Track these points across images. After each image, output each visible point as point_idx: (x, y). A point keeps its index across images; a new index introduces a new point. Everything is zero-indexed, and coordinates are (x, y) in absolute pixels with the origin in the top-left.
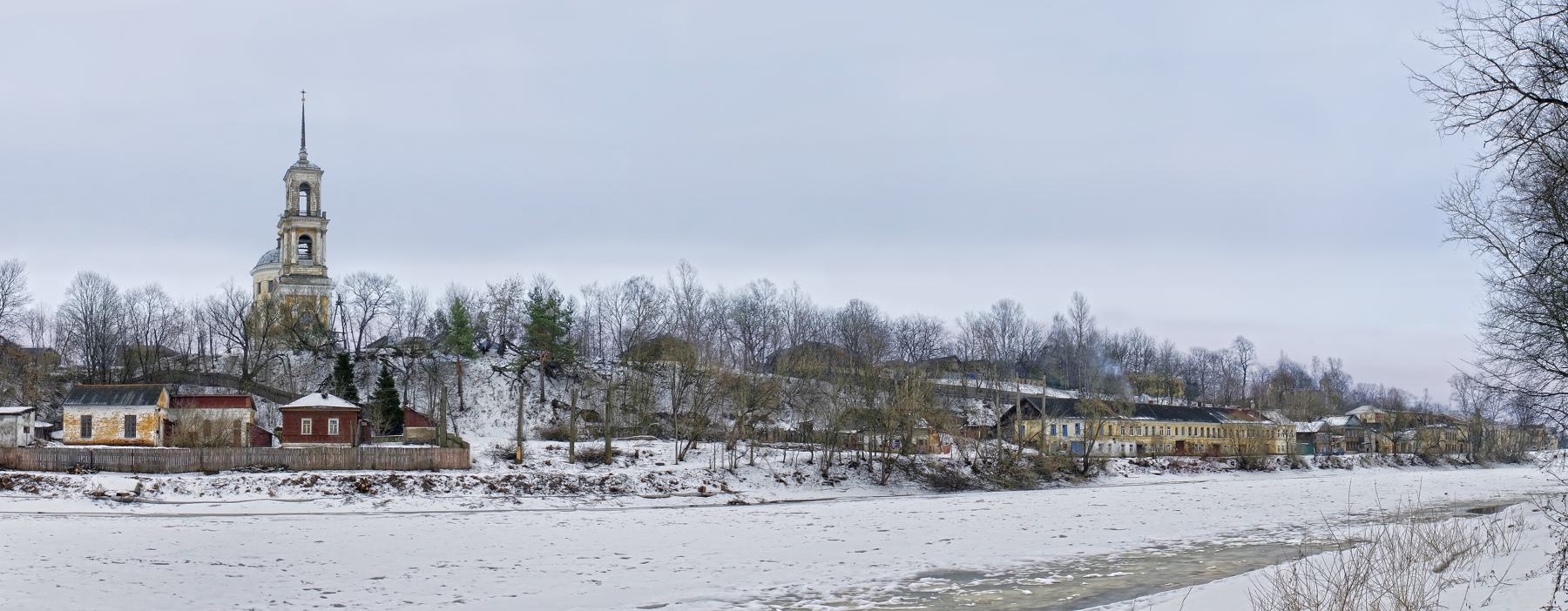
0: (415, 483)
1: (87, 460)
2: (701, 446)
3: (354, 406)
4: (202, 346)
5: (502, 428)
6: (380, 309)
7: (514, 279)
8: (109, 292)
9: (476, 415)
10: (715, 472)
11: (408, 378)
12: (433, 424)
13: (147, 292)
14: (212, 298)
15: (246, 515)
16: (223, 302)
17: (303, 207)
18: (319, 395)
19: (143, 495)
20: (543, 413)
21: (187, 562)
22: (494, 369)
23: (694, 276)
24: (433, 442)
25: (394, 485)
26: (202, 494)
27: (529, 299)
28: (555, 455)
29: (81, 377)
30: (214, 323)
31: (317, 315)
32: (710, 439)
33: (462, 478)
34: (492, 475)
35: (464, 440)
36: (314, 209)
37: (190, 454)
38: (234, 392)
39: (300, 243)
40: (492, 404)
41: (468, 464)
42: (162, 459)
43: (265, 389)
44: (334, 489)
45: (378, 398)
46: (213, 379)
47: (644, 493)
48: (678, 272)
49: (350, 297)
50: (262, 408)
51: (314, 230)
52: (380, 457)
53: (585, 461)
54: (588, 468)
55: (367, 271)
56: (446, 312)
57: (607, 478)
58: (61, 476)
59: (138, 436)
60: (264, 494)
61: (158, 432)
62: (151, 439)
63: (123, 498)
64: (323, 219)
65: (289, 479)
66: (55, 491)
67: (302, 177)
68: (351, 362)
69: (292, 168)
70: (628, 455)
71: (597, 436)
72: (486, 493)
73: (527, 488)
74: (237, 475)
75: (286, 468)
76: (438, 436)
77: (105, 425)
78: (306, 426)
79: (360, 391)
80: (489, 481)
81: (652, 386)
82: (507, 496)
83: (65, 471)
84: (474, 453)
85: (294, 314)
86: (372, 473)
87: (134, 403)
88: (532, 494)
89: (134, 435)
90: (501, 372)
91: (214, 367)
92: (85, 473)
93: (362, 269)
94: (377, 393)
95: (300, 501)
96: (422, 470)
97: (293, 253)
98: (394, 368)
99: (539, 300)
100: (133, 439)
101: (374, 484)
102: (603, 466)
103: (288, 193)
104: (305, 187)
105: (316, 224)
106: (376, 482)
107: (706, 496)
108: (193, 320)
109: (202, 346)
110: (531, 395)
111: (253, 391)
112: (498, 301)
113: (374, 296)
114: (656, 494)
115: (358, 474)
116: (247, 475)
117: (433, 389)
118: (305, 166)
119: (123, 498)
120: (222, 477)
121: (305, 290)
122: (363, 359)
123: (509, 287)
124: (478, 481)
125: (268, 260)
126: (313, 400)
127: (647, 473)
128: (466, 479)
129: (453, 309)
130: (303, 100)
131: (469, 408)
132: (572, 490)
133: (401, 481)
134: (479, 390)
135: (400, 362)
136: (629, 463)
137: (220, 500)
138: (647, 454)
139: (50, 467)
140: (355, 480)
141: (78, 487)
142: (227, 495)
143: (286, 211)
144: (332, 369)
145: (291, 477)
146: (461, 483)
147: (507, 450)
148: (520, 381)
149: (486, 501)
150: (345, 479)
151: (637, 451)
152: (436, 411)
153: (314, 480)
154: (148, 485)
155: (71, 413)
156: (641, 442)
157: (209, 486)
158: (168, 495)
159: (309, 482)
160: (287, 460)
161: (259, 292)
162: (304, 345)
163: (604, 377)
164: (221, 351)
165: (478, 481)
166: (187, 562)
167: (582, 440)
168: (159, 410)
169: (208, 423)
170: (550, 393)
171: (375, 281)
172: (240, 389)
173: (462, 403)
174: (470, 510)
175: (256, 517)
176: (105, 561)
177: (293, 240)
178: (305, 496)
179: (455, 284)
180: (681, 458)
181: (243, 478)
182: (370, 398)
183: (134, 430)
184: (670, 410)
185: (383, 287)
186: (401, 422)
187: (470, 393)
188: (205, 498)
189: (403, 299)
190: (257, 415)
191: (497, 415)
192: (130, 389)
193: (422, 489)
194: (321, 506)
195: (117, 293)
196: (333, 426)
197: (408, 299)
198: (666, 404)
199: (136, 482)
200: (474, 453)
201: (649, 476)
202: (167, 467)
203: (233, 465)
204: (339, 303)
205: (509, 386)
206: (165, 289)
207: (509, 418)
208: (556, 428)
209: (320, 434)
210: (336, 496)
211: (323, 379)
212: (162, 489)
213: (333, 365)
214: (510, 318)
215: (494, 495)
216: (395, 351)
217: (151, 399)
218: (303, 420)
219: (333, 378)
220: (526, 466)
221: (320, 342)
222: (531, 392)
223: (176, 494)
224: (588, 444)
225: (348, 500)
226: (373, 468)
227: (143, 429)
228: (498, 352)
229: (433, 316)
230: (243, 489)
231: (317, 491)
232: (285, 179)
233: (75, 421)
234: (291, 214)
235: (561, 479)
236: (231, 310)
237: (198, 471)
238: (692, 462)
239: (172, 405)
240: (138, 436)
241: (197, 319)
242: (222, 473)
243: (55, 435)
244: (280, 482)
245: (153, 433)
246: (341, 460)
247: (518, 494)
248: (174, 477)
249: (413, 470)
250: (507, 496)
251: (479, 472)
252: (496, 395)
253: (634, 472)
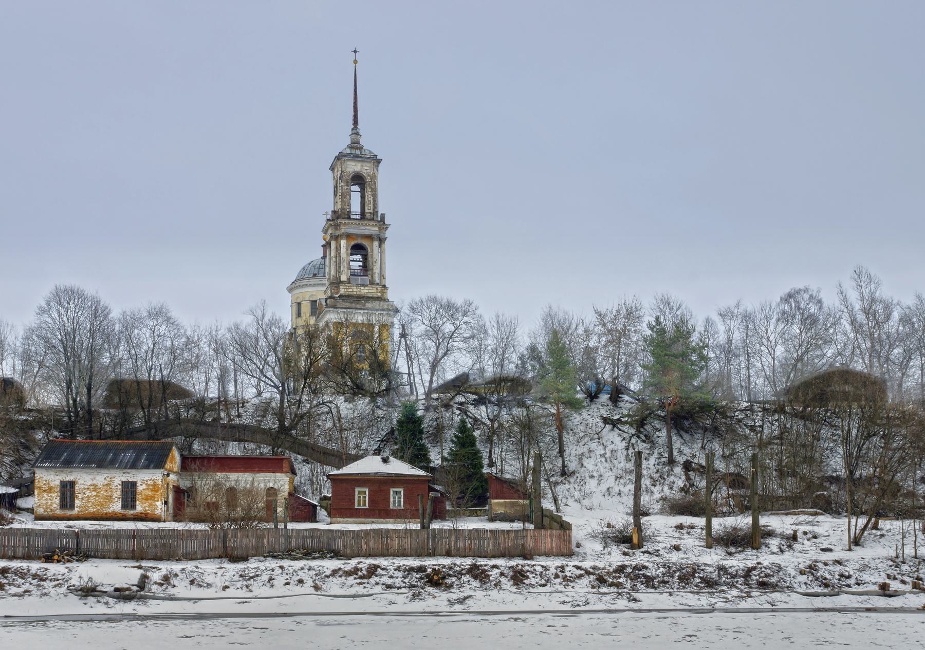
0: (502, 574)
1: (72, 544)
2: (885, 524)
3: (422, 473)
4: (223, 388)
5: (616, 499)
6: (456, 344)
7: (629, 302)
8: (98, 312)
9: (582, 482)
10: (904, 562)
11: (494, 433)
12: (525, 496)
13: (150, 315)
15: (285, 615)
16: (252, 331)
17: (356, 208)
18: (378, 458)
19: (150, 590)
20: (672, 478)
22: (606, 421)
23: (876, 288)
24: (525, 519)
25: (475, 577)
26: (225, 588)
27: (649, 332)
28: (686, 536)
29: (58, 424)
30: (239, 358)
31: (375, 351)
32: (902, 514)
33: (562, 568)
34: (601, 565)
36: (369, 210)
37: (210, 536)
38: (266, 450)
39: (352, 254)
40: (603, 467)
42: (172, 542)
43: (307, 445)
44: (398, 582)
46: (240, 433)
47: (803, 589)
48: (854, 284)
49: (418, 328)
50: (304, 471)
51: (370, 237)
52: (456, 540)
53: (727, 545)
54: (730, 554)
55: (439, 296)
56: (542, 347)
57: (754, 568)
58: (35, 566)
59: (139, 508)
60: (308, 588)
61: (166, 503)
62: (158, 512)
63: (122, 595)
64: (382, 224)
65: (340, 569)
66: (27, 587)
67: (353, 167)
70: (783, 536)
71: (743, 509)
72: (593, 587)
73: (649, 582)
74: (272, 563)
76: (532, 511)
77: (94, 493)
78: (362, 497)
79: (431, 450)
80: (597, 572)
81: (819, 440)
82: (620, 591)
83: (39, 558)
85: (346, 349)
86: (447, 561)
87: (134, 466)
88: (656, 588)
90: (614, 426)
91: (239, 416)
92: (69, 561)
95: (354, 596)
96: (511, 556)
97: (344, 267)
98: (476, 420)
99: (662, 332)
100: (132, 512)
101: (450, 575)
102: (749, 552)
103: (336, 187)
104: (358, 179)
107: (890, 596)
108: (212, 352)
109: (223, 388)
110: (656, 455)
111: (291, 449)
112: (609, 331)
113: (448, 328)
114: (819, 590)
115: (430, 563)
116: (286, 563)
118: (358, 152)
119: (122, 595)
120: (252, 566)
121: (359, 317)
123: (623, 312)
124: (582, 572)
125: (313, 273)
126: (370, 465)
127: (808, 563)
128: (567, 569)
129: (550, 344)
130: (355, 62)
131: (574, 473)
132: (710, 584)
133: (484, 571)
134: (585, 449)
135: (482, 412)
136: (785, 548)
137: (249, 595)
138: (809, 536)
139: (20, 552)
140: (425, 571)
141: (58, 582)
143: (334, 212)
145: (342, 567)
146: (560, 574)
147: (621, 532)
148: (639, 437)
149: (592, 598)
150: (412, 569)
151: (795, 532)
152: (530, 478)
153: (372, 571)
154: (156, 576)
155: (45, 478)
156: (802, 518)
157: (237, 578)
158: (181, 588)
159: (365, 572)
160: (338, 545)
162: (358, 390)
163: (752, 428)
164: (249, 393)
165: (582, 572)
167: (724, 515)
168: (168, 475)
170: (680, 452)
171: (450, 308)
173: (564, 466)
174: (572, 609)
175: (298, 618)
177: (343, 250)
178: (360, 590)
179: (555, 309)
180: (856, 542)
181: (282, 567)
182: (444, 459)
183: (134, 500)
184: (843, 473)
185: (459, 315)
187: (574, 452)
188: (229, 592)
189: (486, 332)
190: (297, 479)
191: (609, 481)
193: (512, 583)
194: (382, 604)
195: (111, 315)
196: (397, 498)
197: (492, 331)
198: (836, 464)
199: (138, 573)
200: (577, 534)
201: (810, 567)
202: (180, 552)
204: (403, 335)
205: (624, 444)
206: (174, 314)
207: (625, 485)
208: (690, 498)
209: (379, 509)
211: (384, 433)
212: (174, 581)
214: (624, 354)
215: (604, 589)
217: (157, 461)
218: (357, 490)
220: (648, 552)
221: (379, 385)
222: (656, 451)
224: (730, 521)
225: (415, 596)
226: (448, 554)
227: (147, 499)
228: (610, 399)
229: (526, 353)
230: (280, 580)
231: (377, 584)
232: (332, 168)
234: (339, 216)
235: (695, 569)
236: (262, 342)
237: (220, 557)
238: (872, 547)
239: (184, 467)
240: (139, 508)
241: (216, 351)
242: (252, 560)
243: (22, 503)
244: (328, 573)
245: (159, 504)
246: (407, 543)
247: (634, 589)
248: (190, 565)
250: (620, 591)
252: (608, 455)
253: (790, 561)
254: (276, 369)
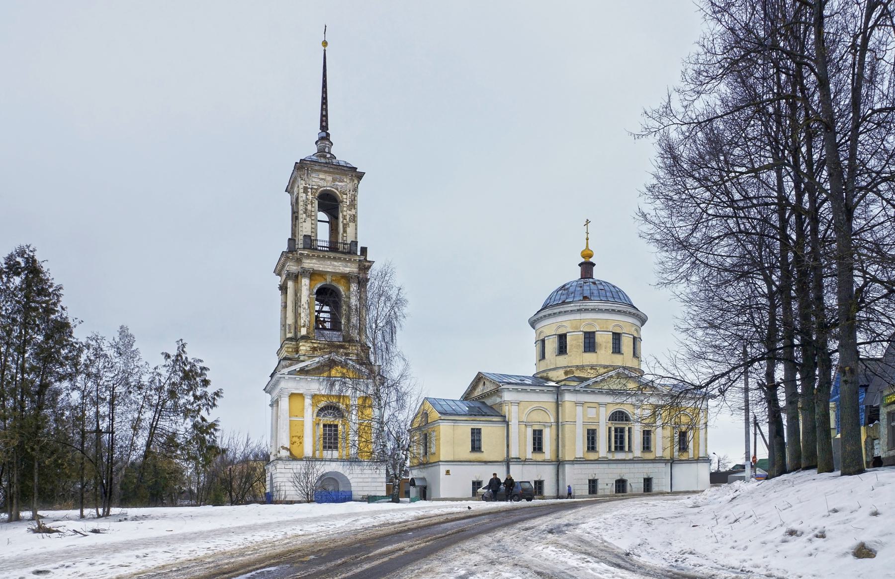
67: (322, 181)
161: (543, 356)
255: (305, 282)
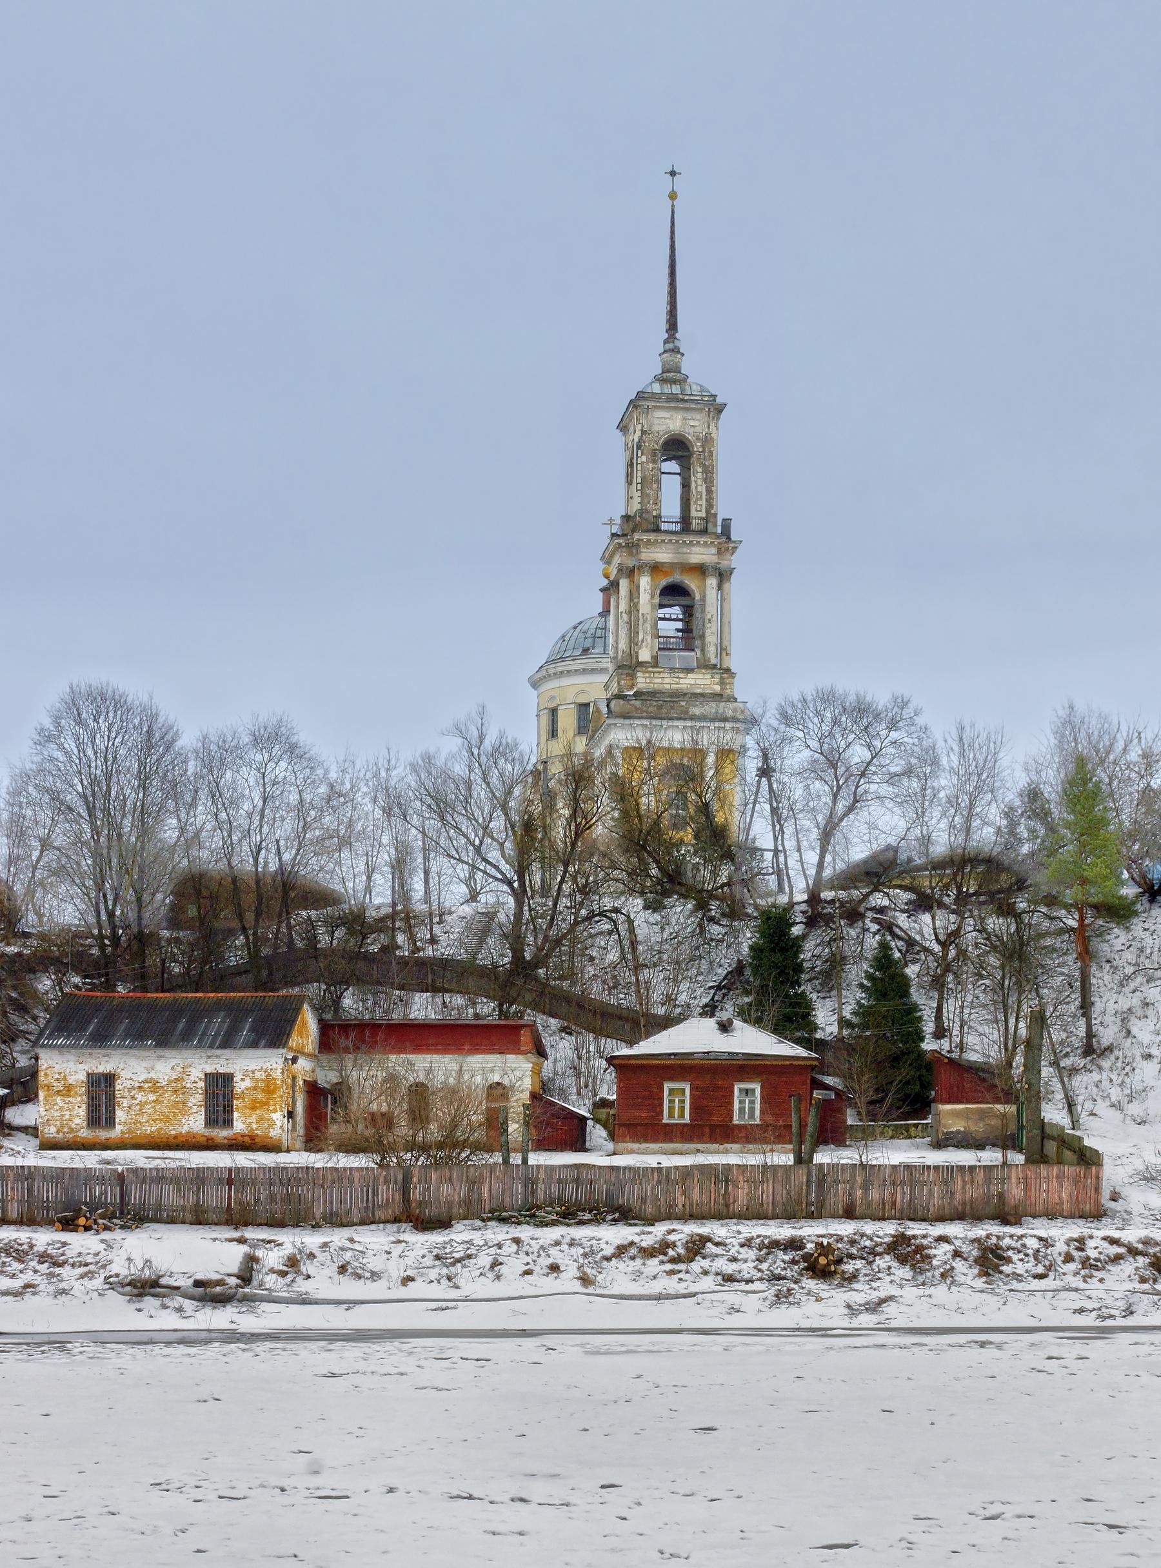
0: (957, 1254)
3: (800, 1051)
4: (402, 886)
6: (873, 787)
9: (1128, 1068)
11: (947, 969)
12: (1009, 1096)
13: (256, 740)
14: (428, 759)
15: (524, 1333)
16: (459, 769)
17: (670, 508)
18: (711, 1023)
19: (261, 1284)
21: (391, 1490)
24: (1007, 1142)
25: (903, 1260)
29: (80, 963)
33: (1081, 1243)
35: (1087, 1143)
36: (697, 512)
38: (487, 1008)
39: (662, 606)
41: (1097, 1202)
42: (306, 1192)
43: (567, 998)
44: (747, 1269)
45: (864, 1026)
50: (561, 1048)
51: (701, 570)
55: (840, 689)
56: (1052, 785)
58: (43, 1238)
59: (240, 1125)
60: (568, 1280)
61: (291, 1115)
62: (275, 1133)
65: (632, 1244)
66: (28, 1277)
67: (668, 422)
68: (796, 930)
69: (641, 395)
72: (1143, 1280)
74: (498, 1233)
75: (625, 1215)
76: (1021, 1128)
77: (152, 1097)
79: (818, 1004)
80: (1152, 1250)
83: (51, 1223)
84: (1113, 1174)
86: (846, 1228)
87: (227, 1042)
89: (229, 1123)
91: (433, 941)
92: (106, 1228)
93: (825, 684)
94: (862, 1011)
95: (659, 1298)
97: (645, 634)
98: (911, 943)
101: (851, 1257)
105: (701, 553)
106: (854, 1251)
109: (402, 886)
111: (536, 1006)
113: (858, 754)
115: (811, 1231)
116: (525, 1232)
117: (1013, 999)
118: (676, 389)
120: (459, 1238)
121: (675, 736)
122: (829, 920)
124: (1122, 1250)
128: (1091, 1244)
130: (673, 196)
133: (920, 1249)
134: (1135, 1001)
137: (454, 1294)
142: (471, 1282)
144: (745, 949)
145: (637, 1239)
146: (1076, 1254)
150: (775, 1244)
154: (272, 1258)
157: (429, 1261)
159: (681, 1250)
160: (628, 1196)
161: (553, 733)
165: (1122, 1250)
166: (391, 1490)
168: (294, 1060)
169: (419, 1092)
172: (503, 1001)
173: (1090, 1035)
174: (1098, 1323)
175: (550, 1340)
176: (198, 1494)
177: (644, 598)
178: (671, 1285)
179: (1080, 707)
181: (517, 1241)
182: (843, 1023)
183: (229, 1109)
185: (881, 728)
186: (927, 1086)
187: (1111, 1007)
188: (413, 1290)
189: (935, 763)
192: (217, 1006)
193: (976, 1271)
194: (713, 1312)
195: (179, 744)
197: (950, 760)
202: (318, 1212)
203: (487, 1208)
210: (750, 1287)
211: (722, 972)
212: (307, 1267)
213: (748, 938)
216: (912, 896)
218: (667, 1086)
219: (748, 972)
221: (715, 874)
223: (345, 1280)
225: (780, 1297)
226: (849, 1213)
227: (253, 1108)
229: (1017, 802)
230: (513, 1266)
231: (705, 1273)
232: (623, 427)
233: (69, 1089)
236: (480, 791)
237: (396, 1220)
239: (326, 1044)
240: (240, 1125)
241: (388, 811)
242: (459, 1226)
244: (609, 1251)
245: (278, 1117)
246: (766, 1193)
248: (337, 1237)
249: (951, 1219)
251: (1126, 1224)
254: (508, 845)
255: (645, 582)
